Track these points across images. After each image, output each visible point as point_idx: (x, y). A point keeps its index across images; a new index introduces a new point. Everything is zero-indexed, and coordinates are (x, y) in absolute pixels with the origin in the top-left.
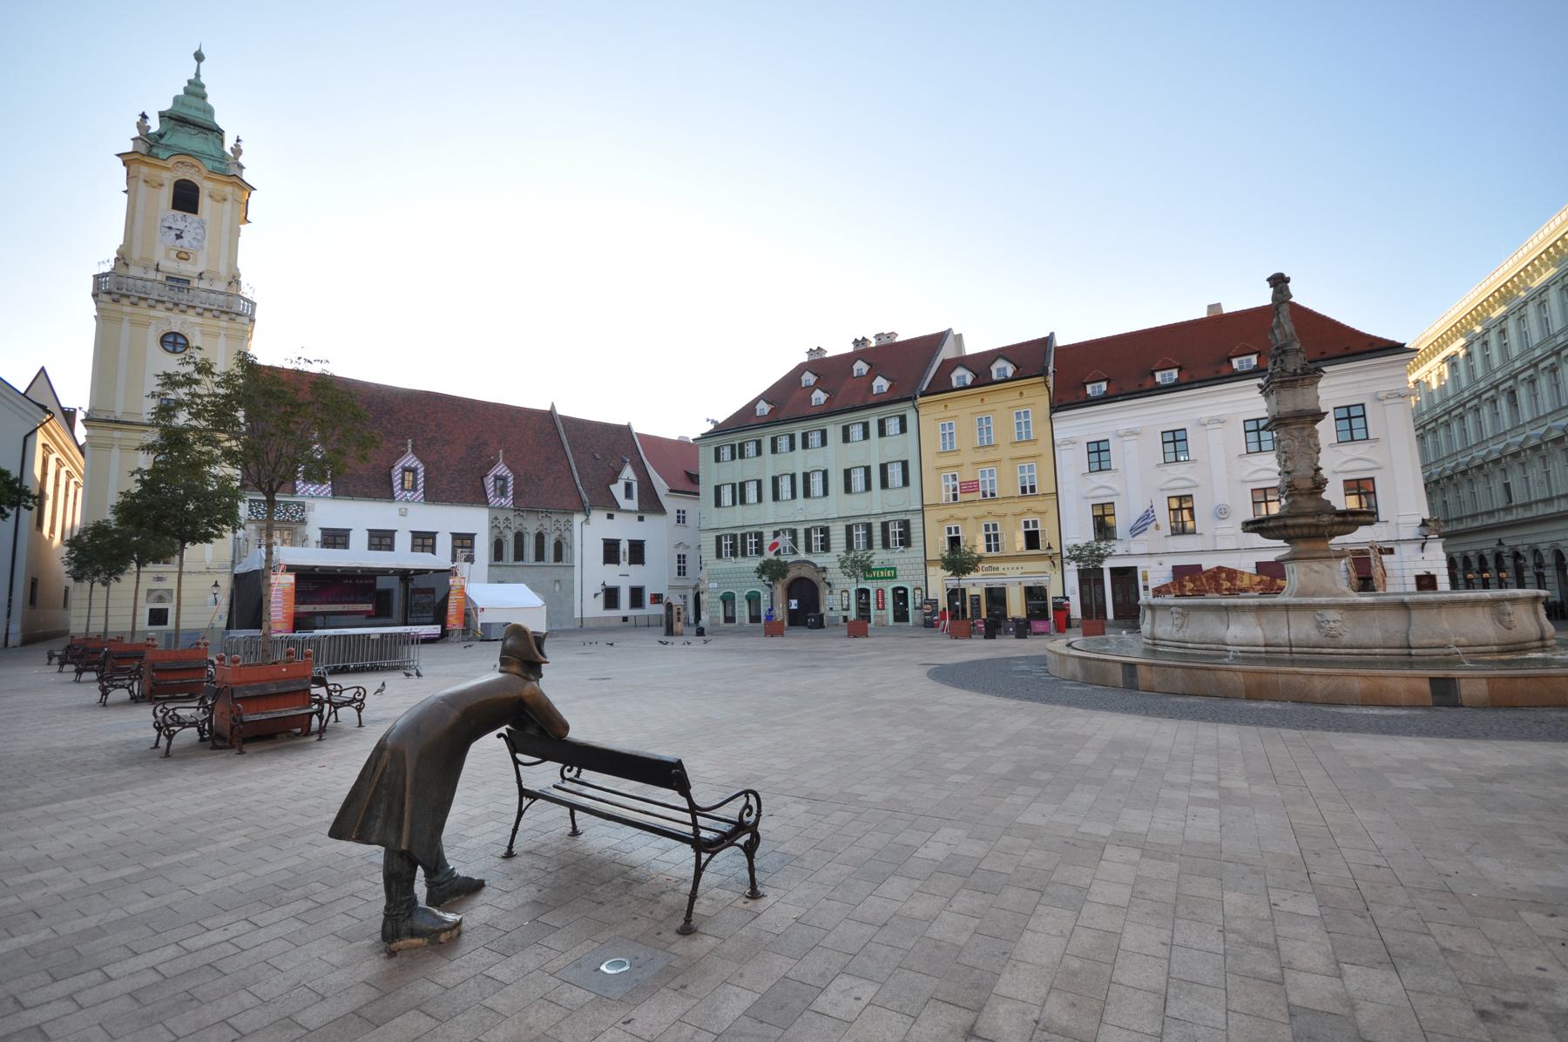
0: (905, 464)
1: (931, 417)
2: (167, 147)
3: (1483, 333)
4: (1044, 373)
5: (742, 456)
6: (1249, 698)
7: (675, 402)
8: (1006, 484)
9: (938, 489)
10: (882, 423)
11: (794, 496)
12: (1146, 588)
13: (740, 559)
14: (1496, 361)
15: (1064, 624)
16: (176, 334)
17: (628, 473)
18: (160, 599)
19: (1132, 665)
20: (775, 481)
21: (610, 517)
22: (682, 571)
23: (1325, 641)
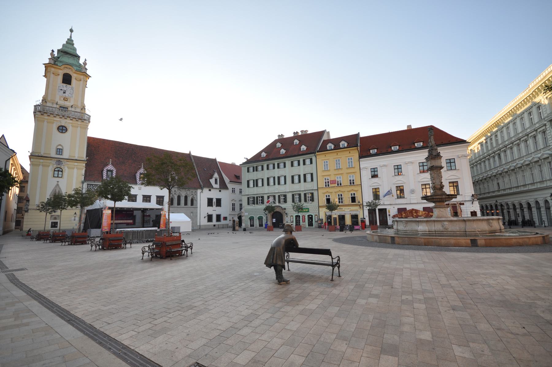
0: (312, 174)
1: (321, 159)
2: (61, 62)
3: (491, 136)
4: (357, 146)
5: (257, 170)
6: (425, 245)
7: (234, 151)
8: (345, 181)
9: (322, 184)
10: (304, 161)
11: (274, 184)
12: (389, 215)
13: (256, 205)
14: (494, 145)
15: (364, 227)
16: (63, 126)
17: (216, 175)
18: (55, 218)
19: (393, 237)
20: (268, 179)
21: (210, 190)
22: (233, 209)
23: (444, 230)
